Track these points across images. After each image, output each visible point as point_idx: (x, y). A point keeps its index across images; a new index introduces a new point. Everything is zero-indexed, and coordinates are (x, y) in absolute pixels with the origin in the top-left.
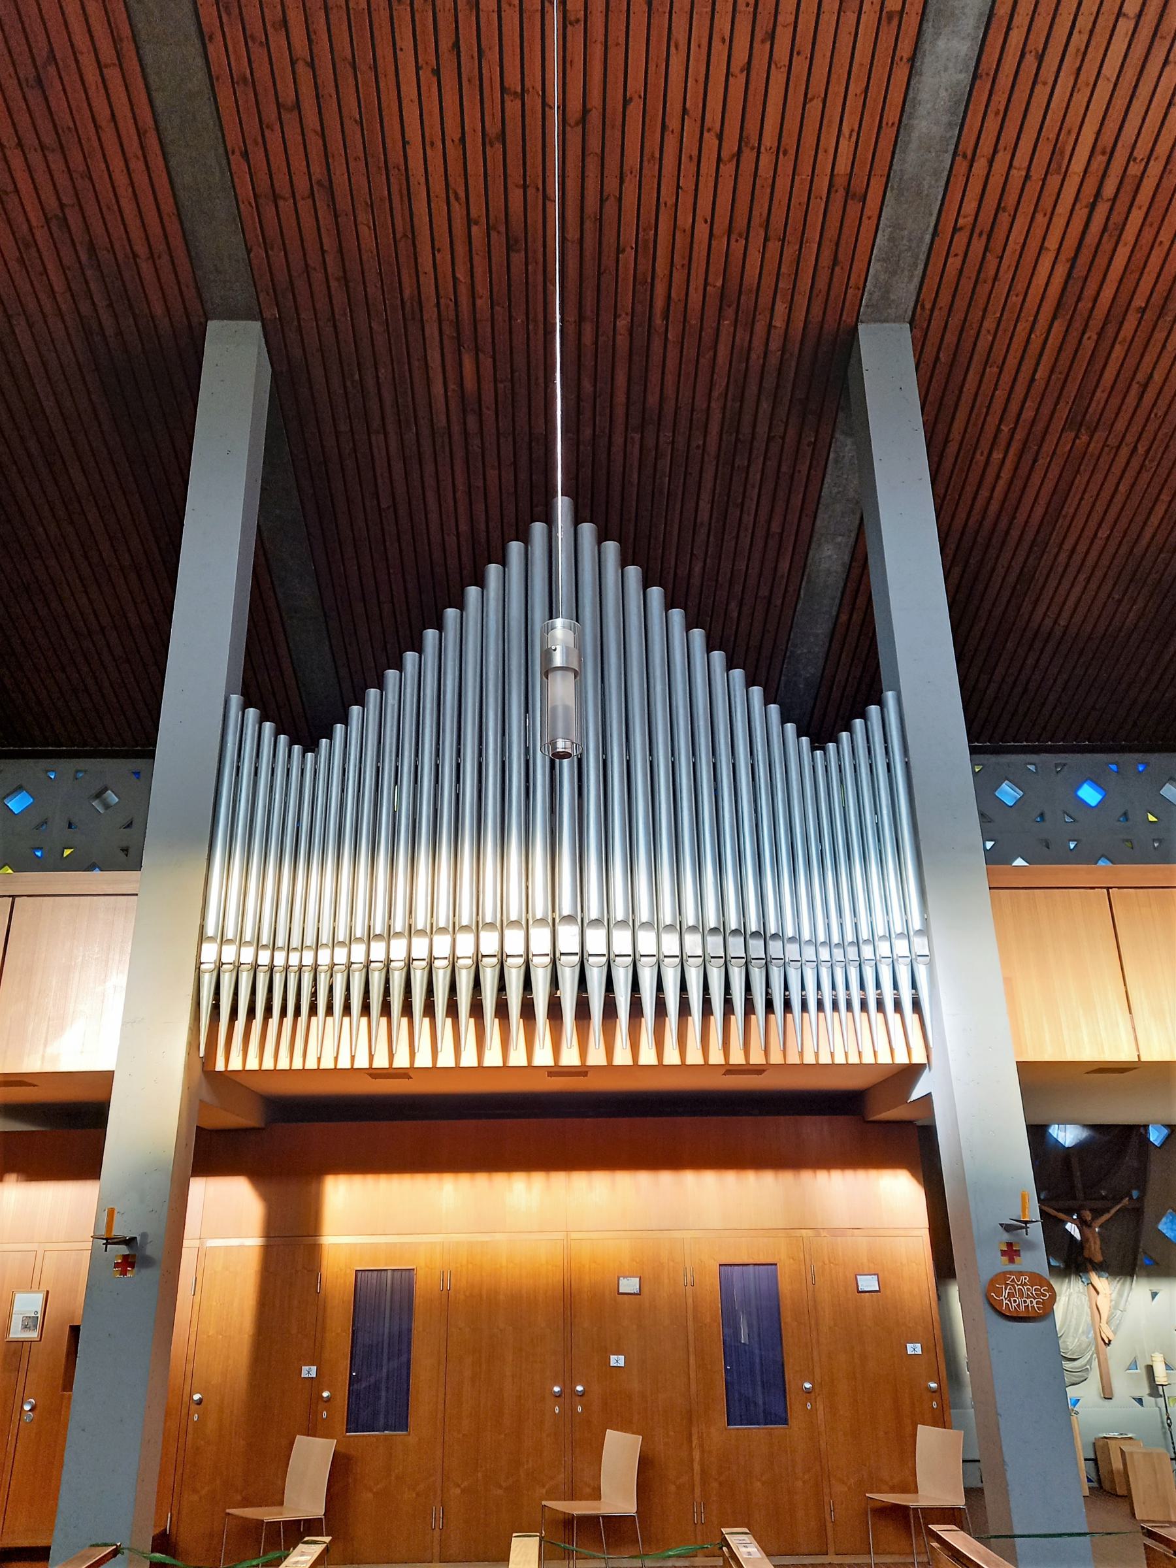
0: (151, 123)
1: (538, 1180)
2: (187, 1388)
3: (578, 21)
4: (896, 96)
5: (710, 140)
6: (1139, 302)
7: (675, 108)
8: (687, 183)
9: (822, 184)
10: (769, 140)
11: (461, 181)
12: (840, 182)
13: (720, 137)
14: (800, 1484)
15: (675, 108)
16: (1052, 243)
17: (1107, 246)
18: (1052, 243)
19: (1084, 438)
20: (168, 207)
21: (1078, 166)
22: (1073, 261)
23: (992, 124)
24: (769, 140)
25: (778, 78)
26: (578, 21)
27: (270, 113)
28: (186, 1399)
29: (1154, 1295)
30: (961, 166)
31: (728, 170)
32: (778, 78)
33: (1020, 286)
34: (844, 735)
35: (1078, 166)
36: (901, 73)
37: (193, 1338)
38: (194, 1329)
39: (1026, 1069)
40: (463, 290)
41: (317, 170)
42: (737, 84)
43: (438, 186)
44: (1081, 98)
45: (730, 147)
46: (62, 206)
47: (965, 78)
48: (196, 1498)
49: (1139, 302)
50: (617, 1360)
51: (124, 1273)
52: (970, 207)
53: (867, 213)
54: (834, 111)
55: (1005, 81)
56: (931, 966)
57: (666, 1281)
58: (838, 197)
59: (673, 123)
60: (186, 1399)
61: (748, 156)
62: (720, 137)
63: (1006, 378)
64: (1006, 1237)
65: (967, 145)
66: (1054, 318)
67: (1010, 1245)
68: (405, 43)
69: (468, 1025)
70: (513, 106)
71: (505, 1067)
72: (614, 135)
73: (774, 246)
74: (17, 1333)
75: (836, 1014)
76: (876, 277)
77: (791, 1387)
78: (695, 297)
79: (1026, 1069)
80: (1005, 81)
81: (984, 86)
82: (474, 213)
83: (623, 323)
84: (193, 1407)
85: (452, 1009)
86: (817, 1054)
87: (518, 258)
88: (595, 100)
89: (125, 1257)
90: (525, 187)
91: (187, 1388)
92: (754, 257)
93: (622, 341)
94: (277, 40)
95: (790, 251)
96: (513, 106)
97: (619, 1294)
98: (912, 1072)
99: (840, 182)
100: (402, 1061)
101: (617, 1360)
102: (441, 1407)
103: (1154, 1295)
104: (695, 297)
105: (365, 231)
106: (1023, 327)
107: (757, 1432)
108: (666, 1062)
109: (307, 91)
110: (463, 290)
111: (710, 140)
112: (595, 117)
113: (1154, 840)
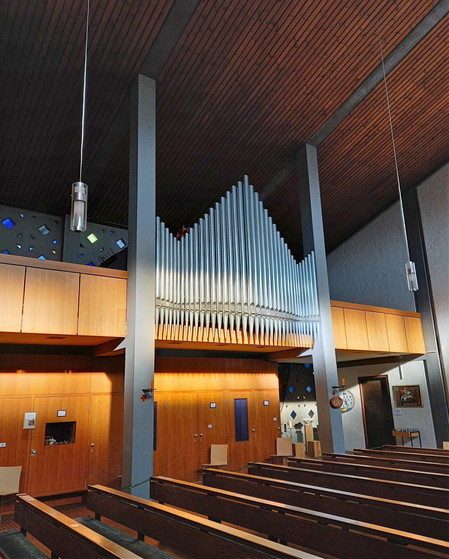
0: (167, 13)
1: (191, 375)
2: (89, 442)
3: (297, 47)
4: (347, 97)
5: (305, 88)
6: (360, 160)
7: (303, 77)
8: (293, 95)
9: (320, 109)
10: (316, 95)
11: (241, 70)
12: (324, 110)
13: (307, 88)
14: (251, 455)
15: (303, 77)
16: (353, 141)
17: (362, 146)
18: (353, 141)
19: (332, 186)
20: (153, 36)
21: (368, 127)
22: (355, 146)
23: (360, 110)
24: (316, 95)
25: (328, 81)
26: (297, 47)
27: (204, 29)
28: (88, 445)
29: (287, 406)
30: (349, 116)
31: (304, 96)
32: (328, 81)
33: (341, 148)
34: (303, 261)
35: (368, 127)
36: (351, 92)
37: (89, 426)
38: (90, 423)
39: (337, 350)
40: (221, 96)
41: (206, 48)
42: (319, 79)
43: (235, 67)
44: (377, 113)
45: (308, 91)
46: (117, 20)
47: (361, 99)
48: (93, 476)
49: (360, 160)
50: (210, 426)
51: (144, 401)
52: (344, 127)
53: (325, 119)
54: (333, 94)
55: (367, 103)
56: (320, 324)
57: (222, 404)
58: (322, 113)
59: (300, 81)
60: (88, 445)
61: (310, 95)
62: (307, 88)
63: (326, 167)
64: (333, 389)
65: (352, 114)
66: (343, 157)
67: (333, 391)
68: (254, 30)
69: (233, 332)
70: (268, 59)
71: (231, 343)
72: (285, 77)
73: (301, 118)
74: (26, 426)
75: (216, 329)
76: (317, 134)
77: (250, 431)
78: (276, 122)
79: (337, 350)
80: (367, 103)
81: (363, 102)
82: (239, 79)
83: (255, 121)
84: (91, 448)
85: (223, 327)
86: (208, 339)
87: (241, 95)
88: (287, 67)
89: (144, 395)
90: (256, 79)
91: (89, 442)
92: (295, 119)
93: (252, 125)
94: (221, 11)
95: (304, 120)
96: (268, 59)
97: (58, 416)
98: (120, 340)
99: (324, 110)
100: (262, 343)
101: (210, 426)
102: (165, 442)
103: (287, 406)
104: (276, 122)
105: (206, 70)
106: (337, 156)
107: (242, 443)
108: (256, 344)
109: (219, 28)
110: (221, 96)
111: (305, 88)
112: (284, 71)
113: (103, 248)
